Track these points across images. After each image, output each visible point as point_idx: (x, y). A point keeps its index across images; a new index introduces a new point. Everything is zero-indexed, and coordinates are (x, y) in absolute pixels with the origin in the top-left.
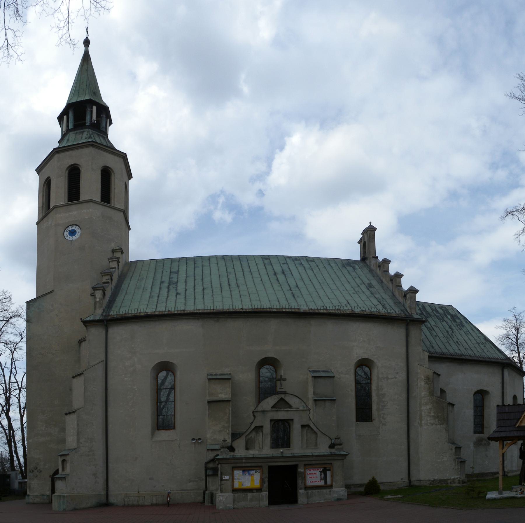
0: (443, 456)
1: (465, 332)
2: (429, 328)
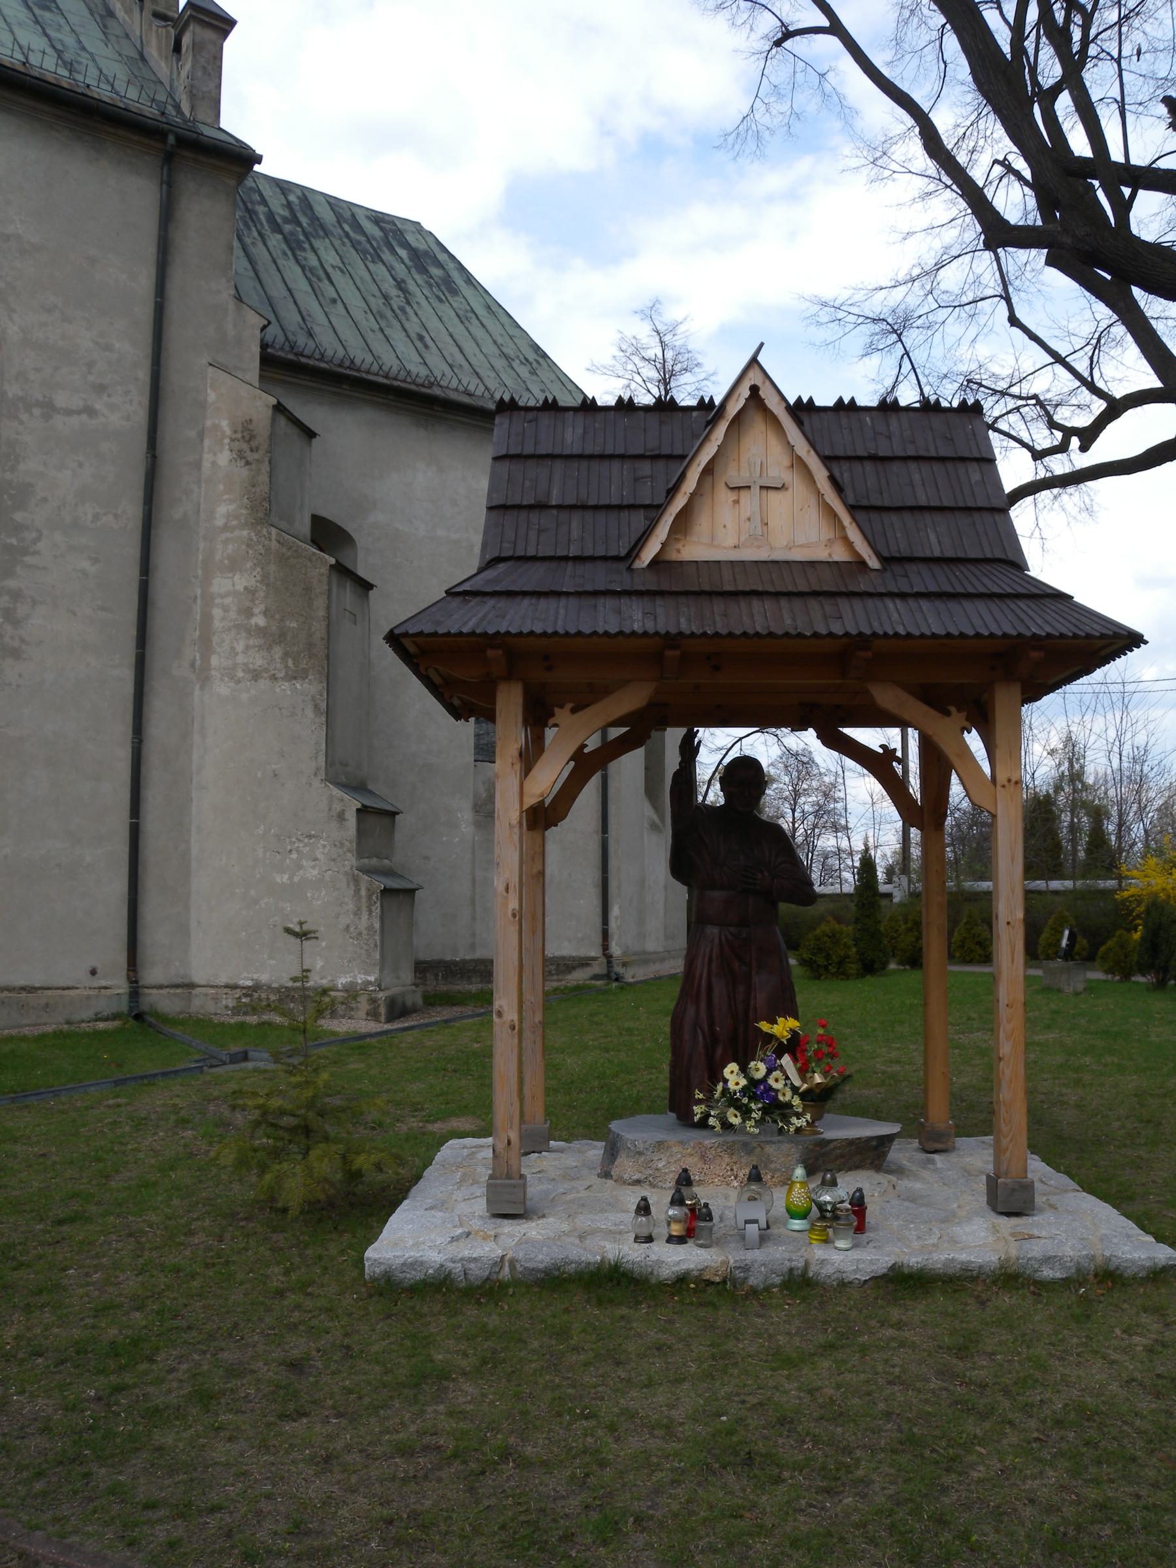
0: (298, 851)
1: (461, 313)
2: (312, 270)
